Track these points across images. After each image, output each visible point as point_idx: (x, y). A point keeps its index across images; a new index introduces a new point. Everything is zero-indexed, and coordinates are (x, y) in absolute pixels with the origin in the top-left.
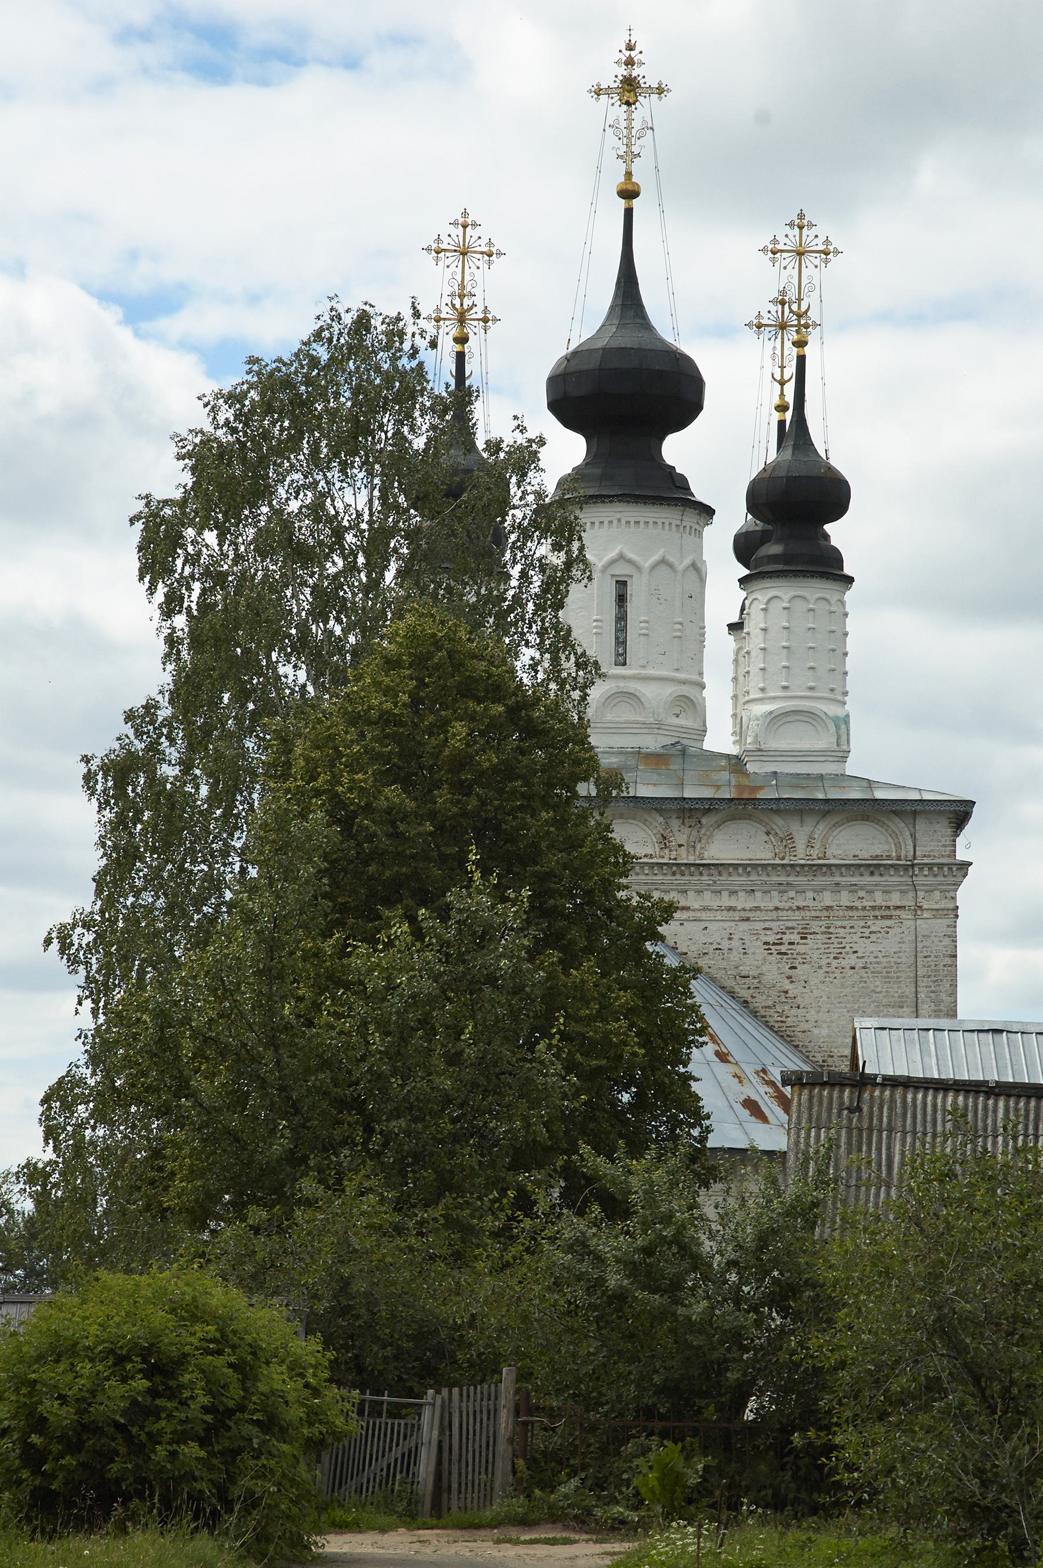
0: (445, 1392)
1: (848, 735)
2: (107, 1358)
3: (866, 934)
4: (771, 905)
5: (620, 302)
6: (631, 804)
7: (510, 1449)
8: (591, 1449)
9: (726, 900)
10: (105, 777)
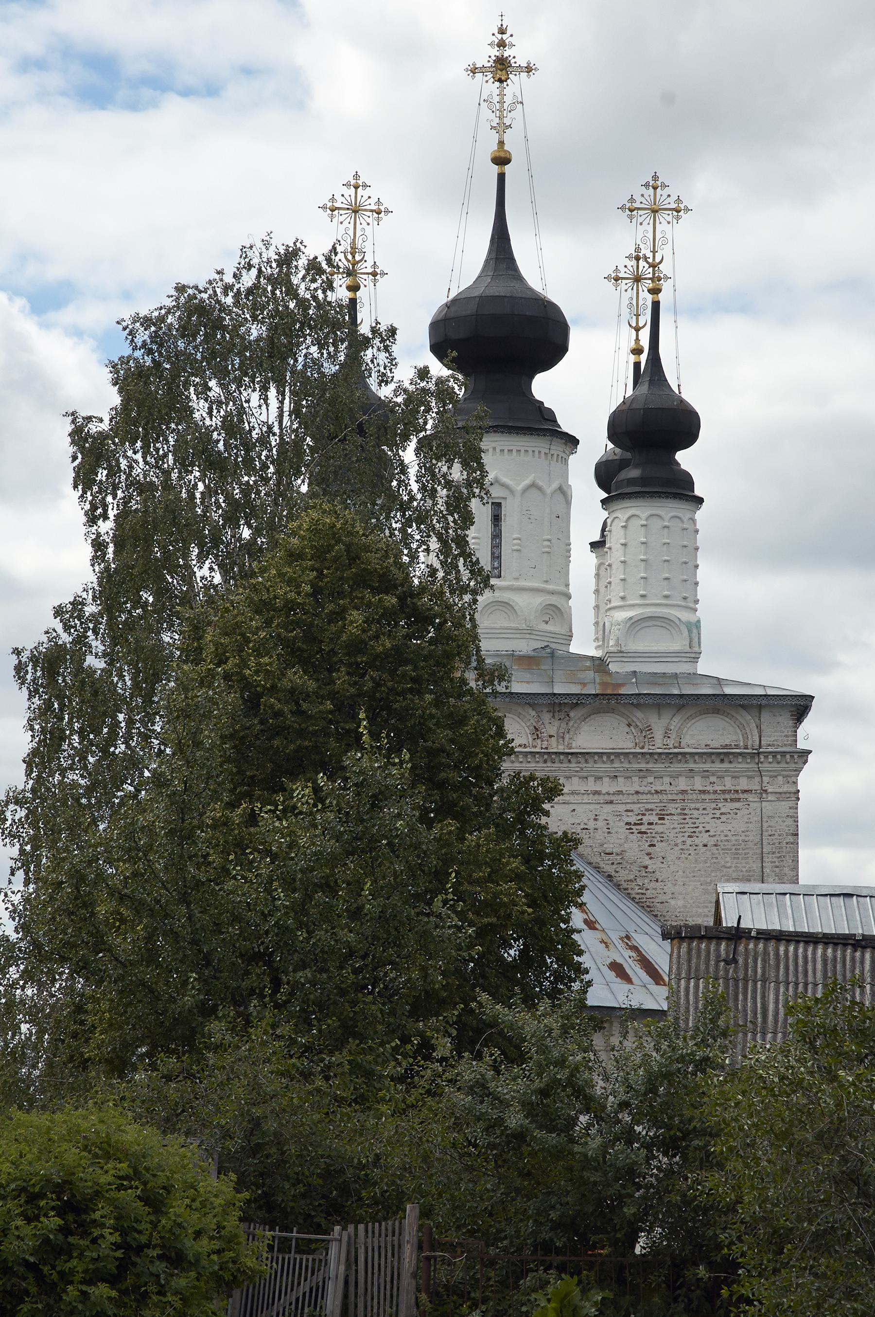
0: (351, 1228)
1: (699, 638)
2: (19, 1196)
3: (718, 816)
4: (632, 790)
5: (493, 255)
6: (507, 700)
7: (414, 1282)
8: (491, 1283)
9: (591, 785)
10: (34, 668)
